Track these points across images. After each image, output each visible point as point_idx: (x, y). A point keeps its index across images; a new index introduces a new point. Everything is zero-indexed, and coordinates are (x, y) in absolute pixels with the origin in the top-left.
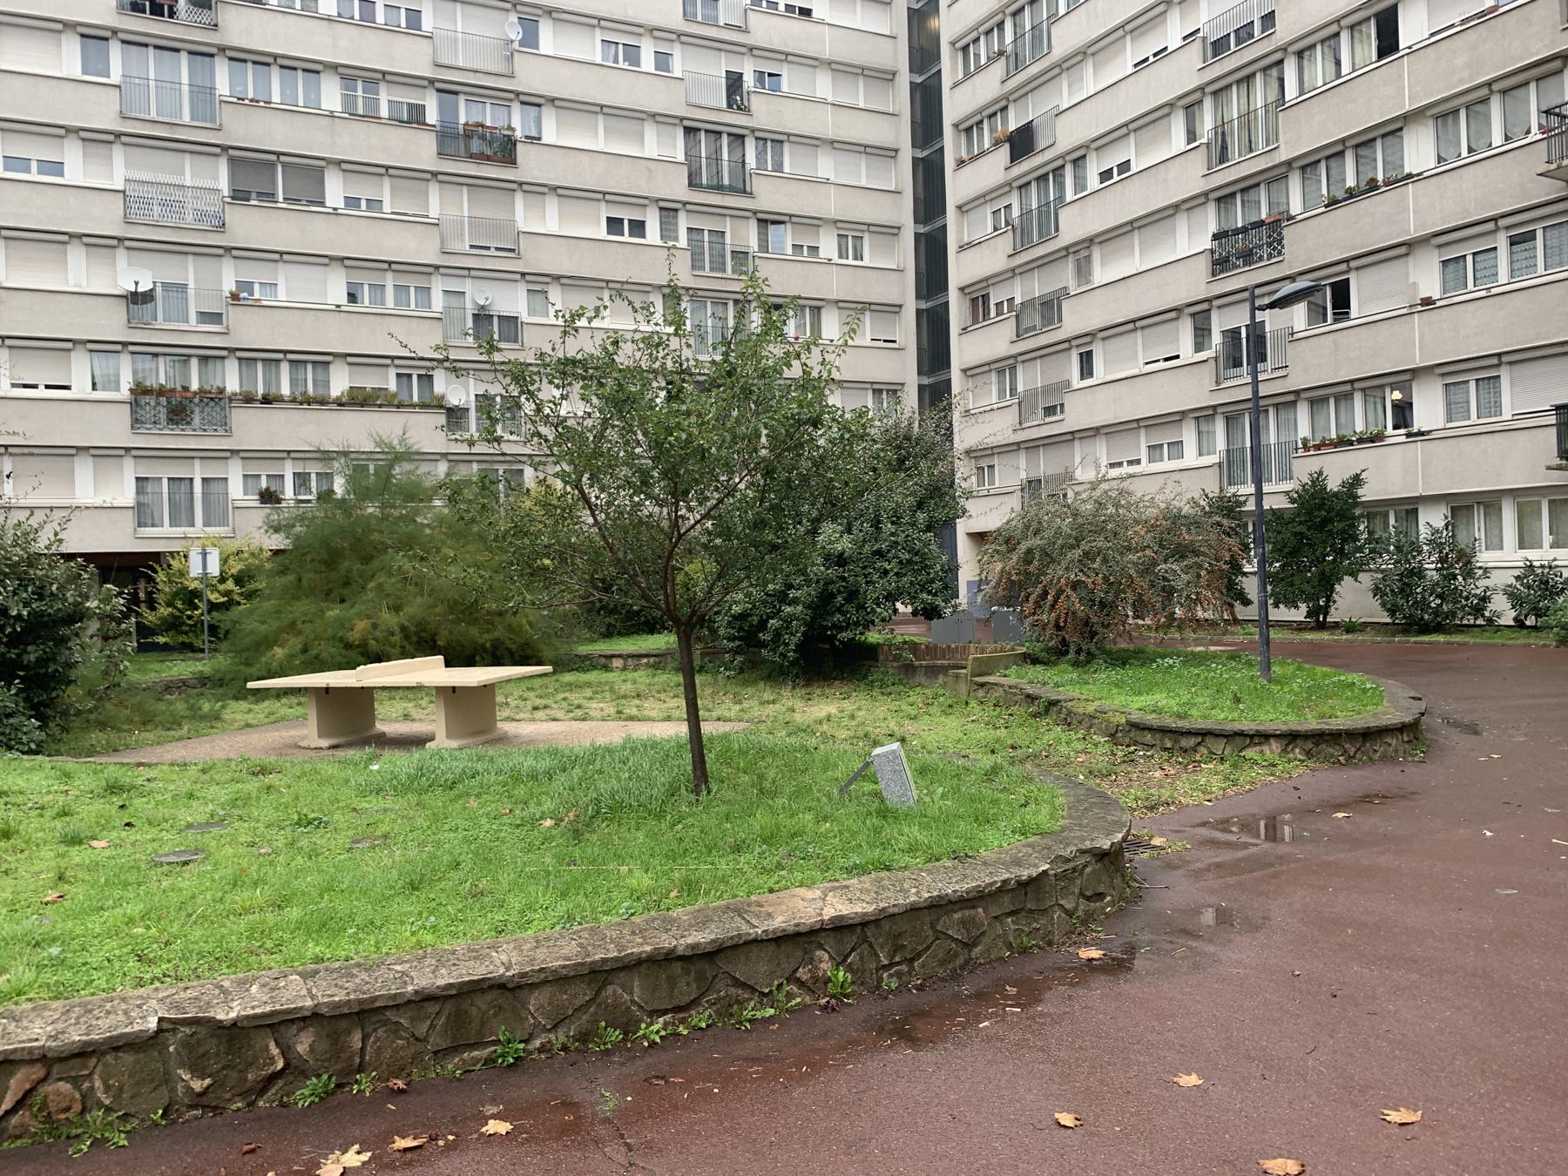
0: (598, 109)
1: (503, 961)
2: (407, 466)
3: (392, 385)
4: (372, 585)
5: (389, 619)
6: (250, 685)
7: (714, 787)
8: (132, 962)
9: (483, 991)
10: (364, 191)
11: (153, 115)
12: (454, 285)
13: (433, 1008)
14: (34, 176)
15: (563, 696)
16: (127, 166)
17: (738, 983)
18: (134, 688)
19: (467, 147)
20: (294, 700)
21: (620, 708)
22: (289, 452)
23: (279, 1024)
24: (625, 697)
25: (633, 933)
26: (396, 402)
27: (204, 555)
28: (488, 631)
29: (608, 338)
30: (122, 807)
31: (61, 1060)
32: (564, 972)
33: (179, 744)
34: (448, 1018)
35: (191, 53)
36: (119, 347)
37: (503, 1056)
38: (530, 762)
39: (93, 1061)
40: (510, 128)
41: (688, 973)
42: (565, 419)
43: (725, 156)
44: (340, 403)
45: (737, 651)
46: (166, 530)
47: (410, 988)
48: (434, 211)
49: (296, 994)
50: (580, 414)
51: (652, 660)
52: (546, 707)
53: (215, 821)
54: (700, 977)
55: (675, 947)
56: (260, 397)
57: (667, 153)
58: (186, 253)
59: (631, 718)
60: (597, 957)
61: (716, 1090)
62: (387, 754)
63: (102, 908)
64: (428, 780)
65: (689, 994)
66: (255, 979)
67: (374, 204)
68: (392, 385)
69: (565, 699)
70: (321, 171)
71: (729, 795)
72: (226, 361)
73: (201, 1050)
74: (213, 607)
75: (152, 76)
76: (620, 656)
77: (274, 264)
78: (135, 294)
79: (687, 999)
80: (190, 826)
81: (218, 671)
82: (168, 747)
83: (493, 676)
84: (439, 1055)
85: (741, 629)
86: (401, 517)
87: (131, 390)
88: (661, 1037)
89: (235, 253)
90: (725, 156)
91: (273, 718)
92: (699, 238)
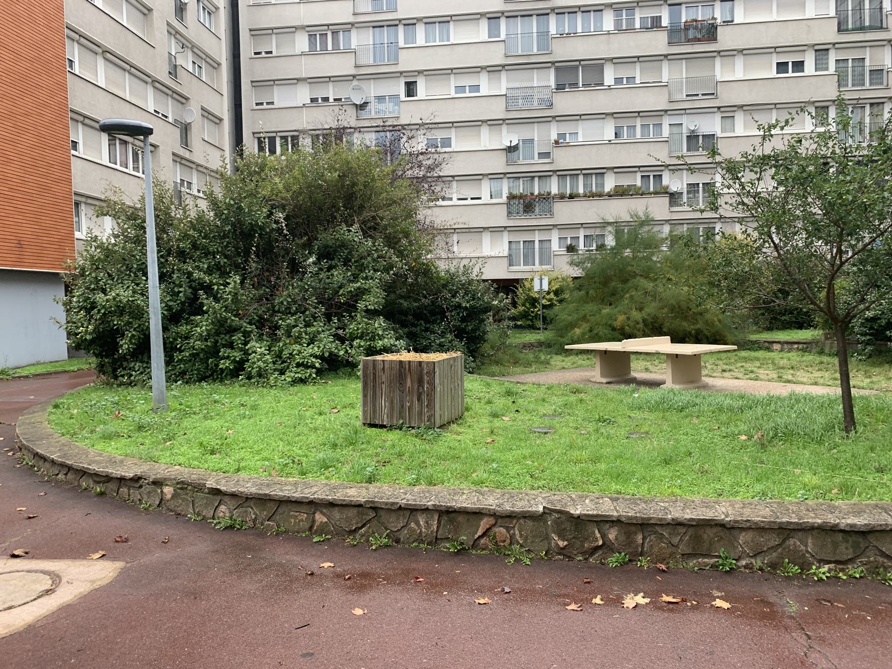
1: (723, 511)
2: (646, 228)
3: (639, 183)
4: (628, 295)
5: (636, 315)
6: (566, 347)
7: (860, 429)
8: (528, 477)
9: (711, 526)
10: (624, 73)
11: (520, 53)
12: (676, 120)
13: (682, 530)
14: (468, 94)
15: (741, 364)
16: (508, 81)
17: (883, 554)
18: (510, 345)
19: (686, 36)
20: (585, 357)
21: (780, 375)
22: (582, 224)
23: (602, 521)
24: (783, 368)
25: (808, 510)
26: (640, 192)
27: (541, 280)
28: (694, 324)
29: (792, 138)
30: (514, 402)
31: (502, 517)
32: (762, 525)
33: (532, 375)
34: (690, 537)
35: (538, 15)
36: (502, 176)
37: (723, 565)
38: (728, 401)
39: (515, 521)
40: (714, 18)
41: (847, 542)
42: (760, 193)
43: (867, 6)
44: (610, 195)
45: (868, 343)
46: (522, 268)
47: (669, 517)
48: (665, 79)
49: (607, 508)
50: (770, 189)
51: (801, 346)
52: (730, 370)
53: (556, 414)
54: (856, 546)
55: (838, 523)
56: (568, 195)
57: (822, 12)
58: (534, 123)
59: (789, 381)
60: (784, 520)
61: (868, 618)
62: (643, 389)
63: (511, 449)
64: (668, 405)
65: (847, 554)
66: (587, 497)
67: (631, 79)
68: (639, 183)
69: (742, 367)
70: (602, 65)
71: (869, 435)
72: (552, 178)
73: (563, 527)
74: (544, 307)
75: (519, 32)
76: (779, 342)
77: (576, 122)
78: (510, 147)
79: (845, 558)
80: (545, 415)
81: (548, 339)
82: (527, 376)
83: (700, 350)
84: (685, 556)
85: (871, 328)
86: (643, 257)
87: (507, 197)
88: (827, 577)
89: (557, 119)
90: (867, 6)
91: (575, 365)
92: (844, 65)
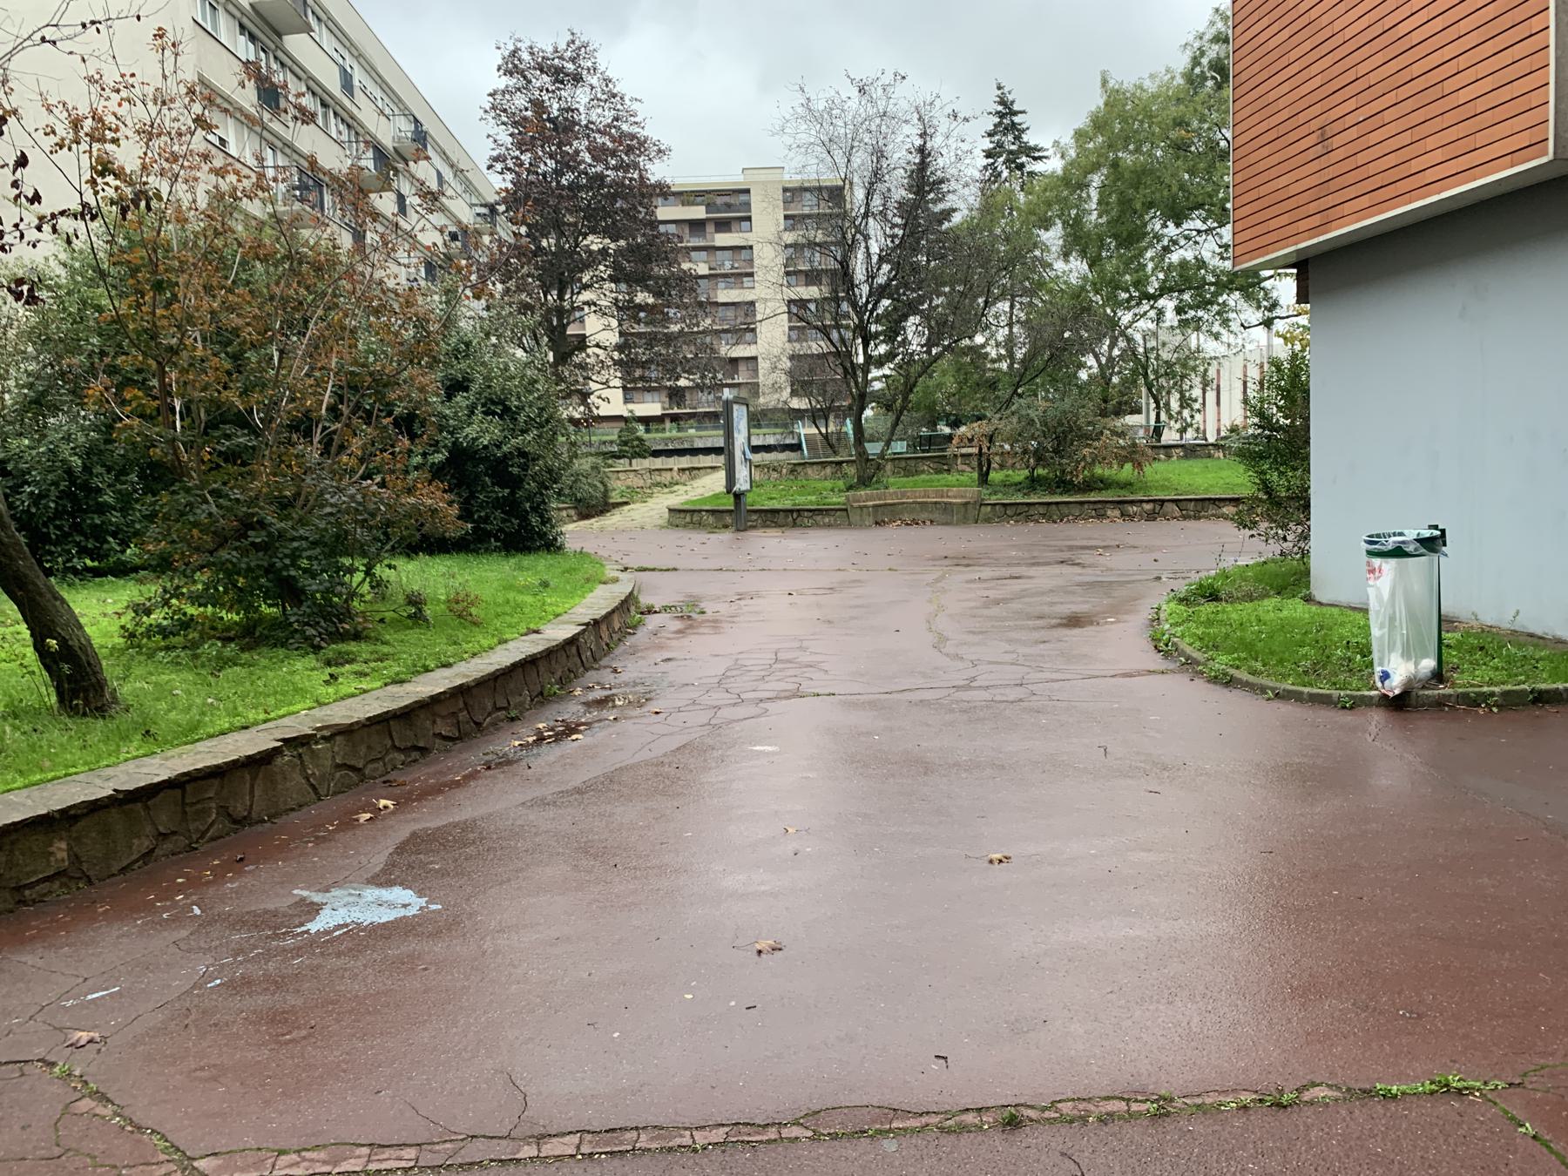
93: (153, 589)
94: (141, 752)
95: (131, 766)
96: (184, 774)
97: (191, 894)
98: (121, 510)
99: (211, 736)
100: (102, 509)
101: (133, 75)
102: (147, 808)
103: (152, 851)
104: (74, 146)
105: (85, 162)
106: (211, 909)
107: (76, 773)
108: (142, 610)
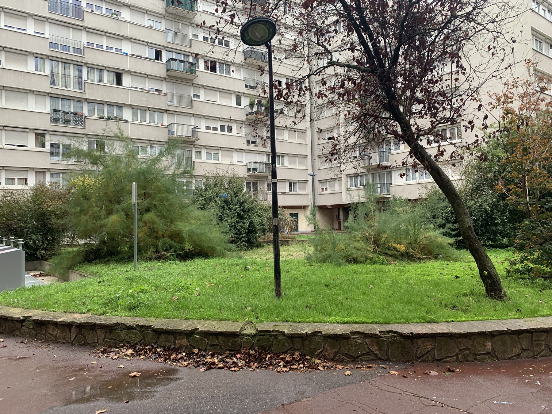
0: (147, 76)
35: (74, 64)
93: (517, 256)
94: (516, 316)
95: (513, 321)
96: (533, 329)
97: (536, 376)
98: (503, 225)
99: (542, 316)
100: (496, 225)
101: (518, 78)
102: (518, 338)
103: (520, 354)
104: (498, 107)
105: (501, 111)
106: (544, 384)
107: (494, 319)
108: (514, 263)
